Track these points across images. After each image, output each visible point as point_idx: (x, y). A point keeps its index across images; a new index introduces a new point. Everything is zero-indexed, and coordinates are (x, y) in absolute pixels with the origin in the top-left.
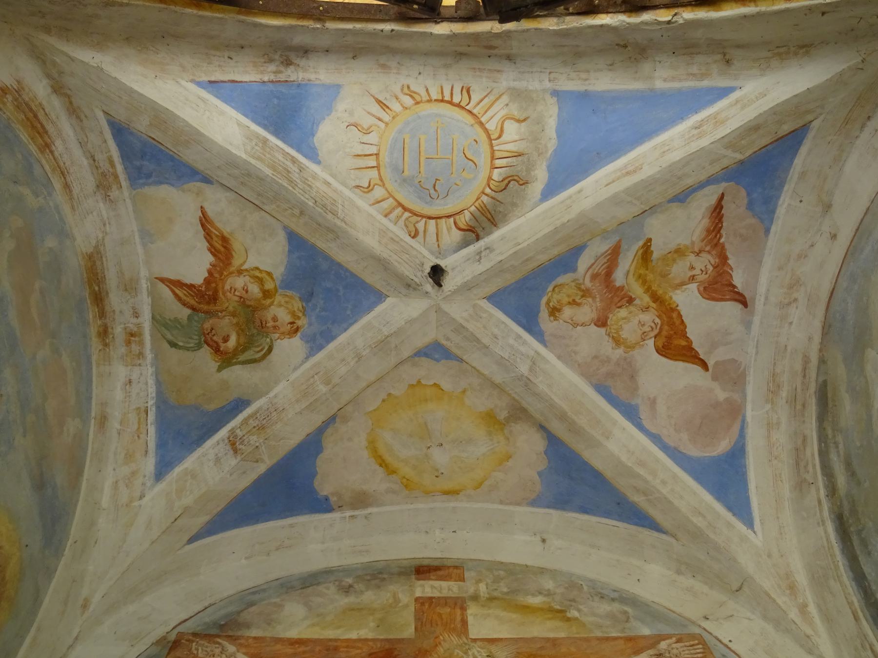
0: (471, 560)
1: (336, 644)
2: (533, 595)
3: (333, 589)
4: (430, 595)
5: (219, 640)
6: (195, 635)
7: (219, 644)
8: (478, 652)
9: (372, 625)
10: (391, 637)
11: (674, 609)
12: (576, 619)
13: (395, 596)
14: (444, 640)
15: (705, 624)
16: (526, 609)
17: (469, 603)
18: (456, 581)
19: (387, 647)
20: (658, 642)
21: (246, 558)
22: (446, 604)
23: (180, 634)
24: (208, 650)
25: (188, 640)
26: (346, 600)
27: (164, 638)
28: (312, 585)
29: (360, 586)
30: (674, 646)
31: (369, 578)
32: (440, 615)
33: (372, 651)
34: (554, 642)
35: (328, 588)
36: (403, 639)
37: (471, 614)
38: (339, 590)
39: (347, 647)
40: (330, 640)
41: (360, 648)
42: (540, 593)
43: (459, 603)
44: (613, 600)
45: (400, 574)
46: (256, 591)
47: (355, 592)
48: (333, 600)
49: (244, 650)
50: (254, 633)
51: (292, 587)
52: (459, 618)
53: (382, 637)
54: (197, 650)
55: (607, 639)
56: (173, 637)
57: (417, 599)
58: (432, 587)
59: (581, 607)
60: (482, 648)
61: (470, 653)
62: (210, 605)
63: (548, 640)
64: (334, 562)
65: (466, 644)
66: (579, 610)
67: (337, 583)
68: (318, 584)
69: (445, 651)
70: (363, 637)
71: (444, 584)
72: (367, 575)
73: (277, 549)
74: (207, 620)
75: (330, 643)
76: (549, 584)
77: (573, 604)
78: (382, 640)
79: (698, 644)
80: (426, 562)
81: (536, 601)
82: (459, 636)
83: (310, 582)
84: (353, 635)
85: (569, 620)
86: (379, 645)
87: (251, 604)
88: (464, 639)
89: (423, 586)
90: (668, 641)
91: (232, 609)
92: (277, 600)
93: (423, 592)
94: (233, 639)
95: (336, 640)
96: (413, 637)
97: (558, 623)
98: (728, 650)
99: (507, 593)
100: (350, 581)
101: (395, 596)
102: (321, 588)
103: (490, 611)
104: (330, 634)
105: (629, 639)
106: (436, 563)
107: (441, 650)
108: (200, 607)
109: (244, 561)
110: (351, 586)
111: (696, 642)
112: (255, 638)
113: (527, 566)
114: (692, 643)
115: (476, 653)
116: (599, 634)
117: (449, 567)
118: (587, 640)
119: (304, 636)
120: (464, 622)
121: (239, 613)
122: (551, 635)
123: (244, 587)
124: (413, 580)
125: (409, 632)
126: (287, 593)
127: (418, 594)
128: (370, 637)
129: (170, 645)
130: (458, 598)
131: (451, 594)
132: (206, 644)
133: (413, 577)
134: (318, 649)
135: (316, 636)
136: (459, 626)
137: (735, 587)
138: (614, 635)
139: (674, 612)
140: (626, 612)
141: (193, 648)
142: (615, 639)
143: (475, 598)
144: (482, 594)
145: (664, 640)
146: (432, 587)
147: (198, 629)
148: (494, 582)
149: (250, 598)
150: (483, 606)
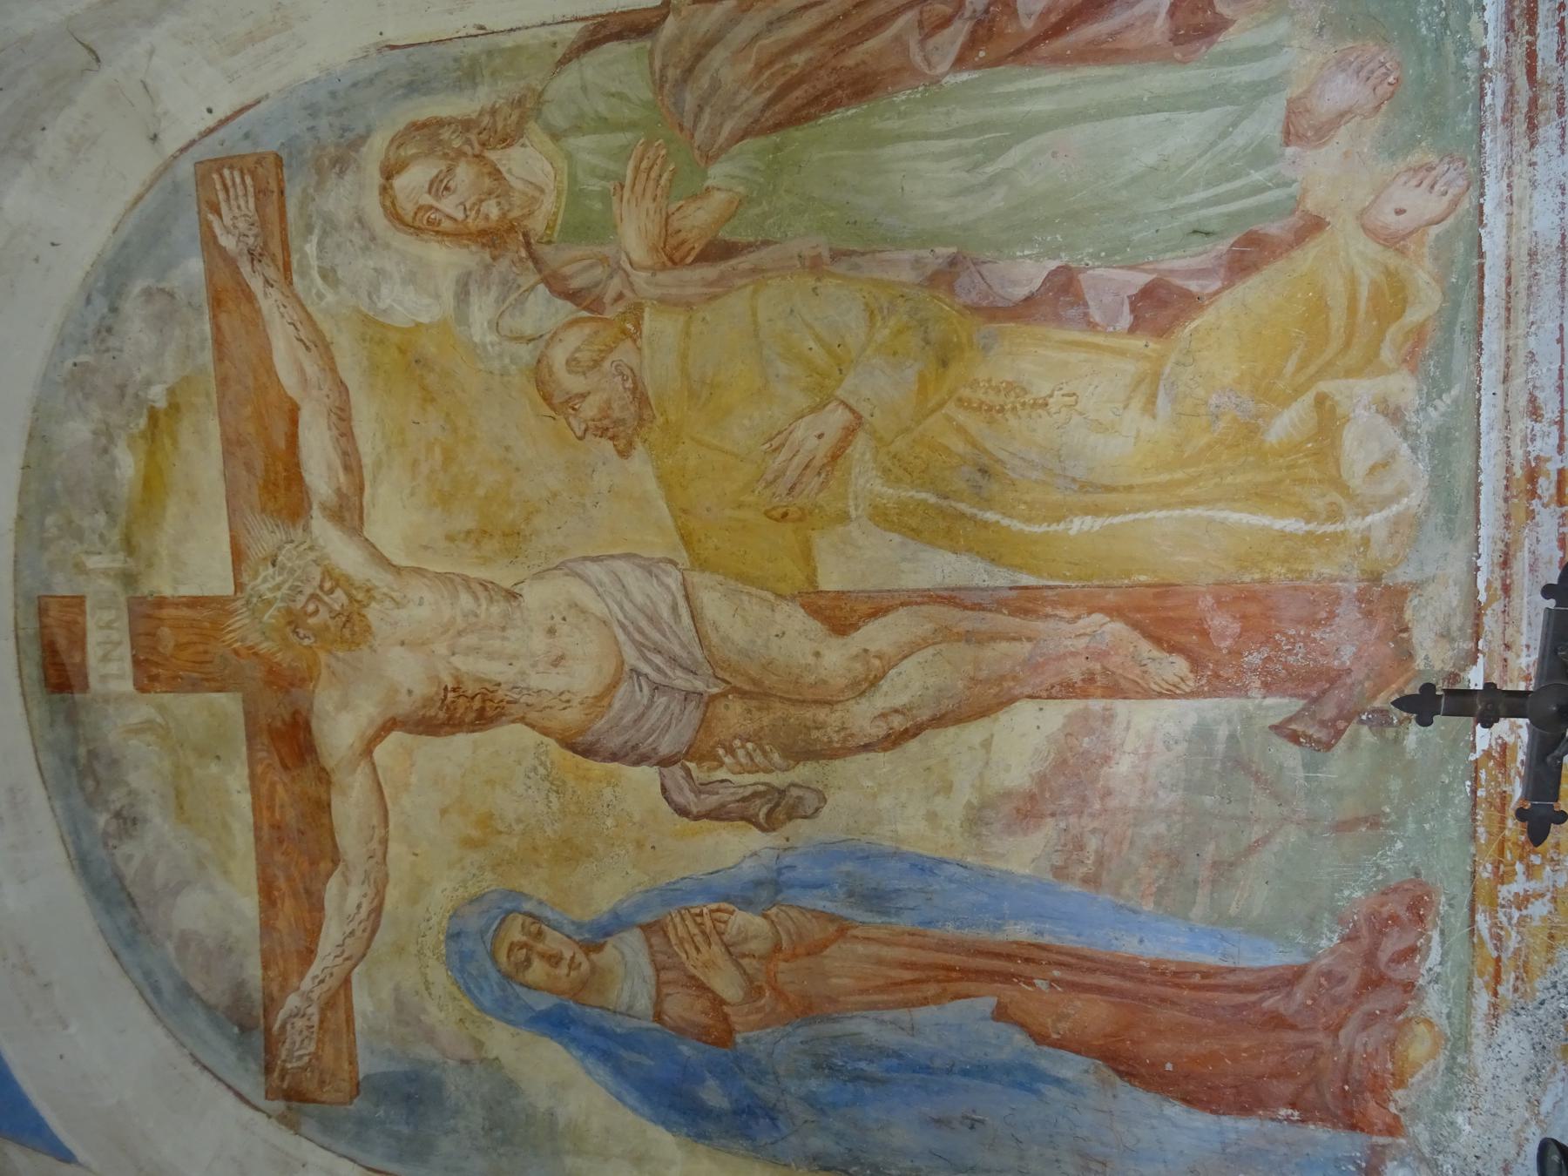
0: (16, 580)
1: (266, 827)
2: (113, 464)
3: (127, 847)
4: (128, 665)
5: (276, 1027)
6: (268, 1070)
7: (283, 1027)
8: (265, 580)
9: (214, 769)
10: (242, 735)
11: (129, 197)
12: (171, 392)
13: (137, 731)
14: (243, 640)
15: (171, 145)
16: (153, 486)
17: (144, 590)
18: (83, 613)
19: (265, 739)
20: (222, 250)
21: (66, 1027)
22: (151, 634)
23: (270, 1094)
24: (298, 1039)
25: (282, 1078)
26: (158, 820)
27: (283, 1119)
28: (123, 888)
29: (117, 798)
30: (227, 220)
31: (90, 784)
32: (179, 647)
33: (278, 765)
34: (232, 445)
35: (129, 858)
36: (247, 714)
37: (175, 589)
38: (131, 837)
39: (271, 808)
40: (258, 839)
41: (273, 785)
42: (105, 451)
43: (146, 615)
44: (114, 310)
45: (72, 719)
46: (150, 991)
47: (132, 806)
48: (160, 842)
49: (294, 980)
50: (253, 971)
51: (133, 923)
52: (185, 612)
53: (244, 749)
54: (301, 1057)
55: (219, 342)
56: (279, 1105)
57: (141, 689)
58: (105, 658)
59: (139, 377)
60: (256, 574)
61: (269, 595)
62: (196, 1061)
63: (227, 454)
64: (53, 852)
65: (248, 602)
66: (148, 383)
67: (112, 842)
68: (119, 877)
69: (267, 639)
70: (247, 783)
71: (93, 638)
72: (82, 789)
73: (33, 972)
74: (231, 1057)
75: (266, 837)
76: (77, 431)
77: (130, 391)
78: (250, 748)
79: (222, 176)
80: (33, 671)
81: (128, 465)
82: (232, 613)
83: (118, 900)
84: (244, 800)
85: (174, 408)
86: (264, 754)
87: (186, 990)
88: (238, 604)
89: (104, 678)
90: (218, 231)
91: (200, 1021)
92: (170, 947)
93: (120, 677)
94: (271, 1004)
95: (257, 828)
96: (239, 695)
97: (185, 427)
98: (233, 124)
99: (112, 518)
100: (102, 819)
101: (137, 731)
102: (130, 872)
103: (164, 553)
104: (243, 840)
105: (217, 302)
106: (34, 652)
107: (265, 647)
108: (205, 1081)
109: (72, 1030)
110: (118, 815)
111: (215, 176)
112: (266, 967)
113: (26, 467)
114: (219, 186)
115: (268, 585)
116: (207, 356)
117: (43, 627)
118: (223, 382)
119: (254, 885)
120: (194, 602)
121: (209, 1008)
122: (216, 447)
123: (144, 1015)
124: (88, 696)
125: (229, 704)
126: (148, 932)
127: (128, 686)
128: (246, 771)
129: (295, 1104)
130: (130, 611)
131: (124, 623)
132: (287, 1045)
133: (78, 696)
134: (279, 857)
135: (252, 865)
136: (206, 613)
137: (83, 56)
138: (207, 327)
139: (140, 198)
140: (148, 294)
141: (300, 1064)
142: (217, 328)
143: (128, 579)
144: (118, 565)
145: (215, 237)
146: (105, 658)
147: (255, 1067)
148: (81, 539)
149: (169, 997)
150: (150, 565)
